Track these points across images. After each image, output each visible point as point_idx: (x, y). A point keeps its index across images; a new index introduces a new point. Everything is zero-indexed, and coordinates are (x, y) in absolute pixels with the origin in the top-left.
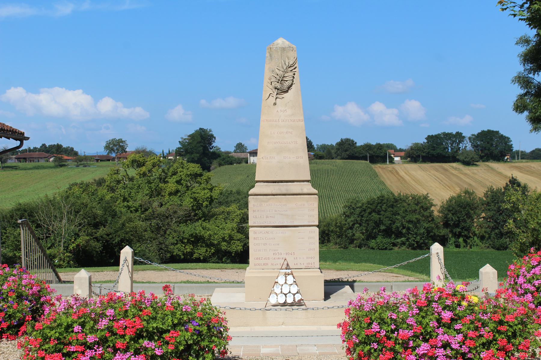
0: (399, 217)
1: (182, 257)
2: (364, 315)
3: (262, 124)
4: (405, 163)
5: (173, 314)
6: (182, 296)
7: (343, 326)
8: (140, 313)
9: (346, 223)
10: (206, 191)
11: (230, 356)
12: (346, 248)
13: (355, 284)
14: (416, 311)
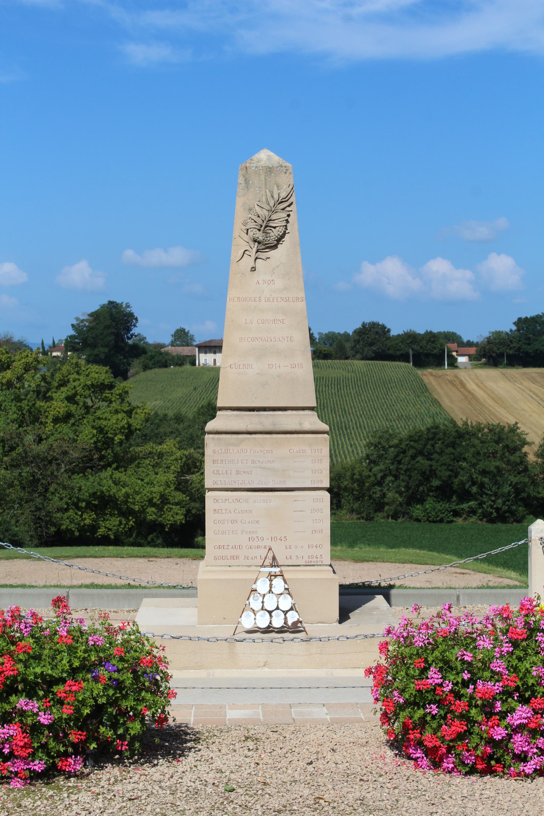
1: (77, 534)
3: (230, 305)
4: (476, 366)
5: (72, 650)
6: (85, 614)
8: (12, 648)
9: (371, 474)
10: (120, 416)
12: (369, 519)
13: (393, 592)
14: (507, 648)
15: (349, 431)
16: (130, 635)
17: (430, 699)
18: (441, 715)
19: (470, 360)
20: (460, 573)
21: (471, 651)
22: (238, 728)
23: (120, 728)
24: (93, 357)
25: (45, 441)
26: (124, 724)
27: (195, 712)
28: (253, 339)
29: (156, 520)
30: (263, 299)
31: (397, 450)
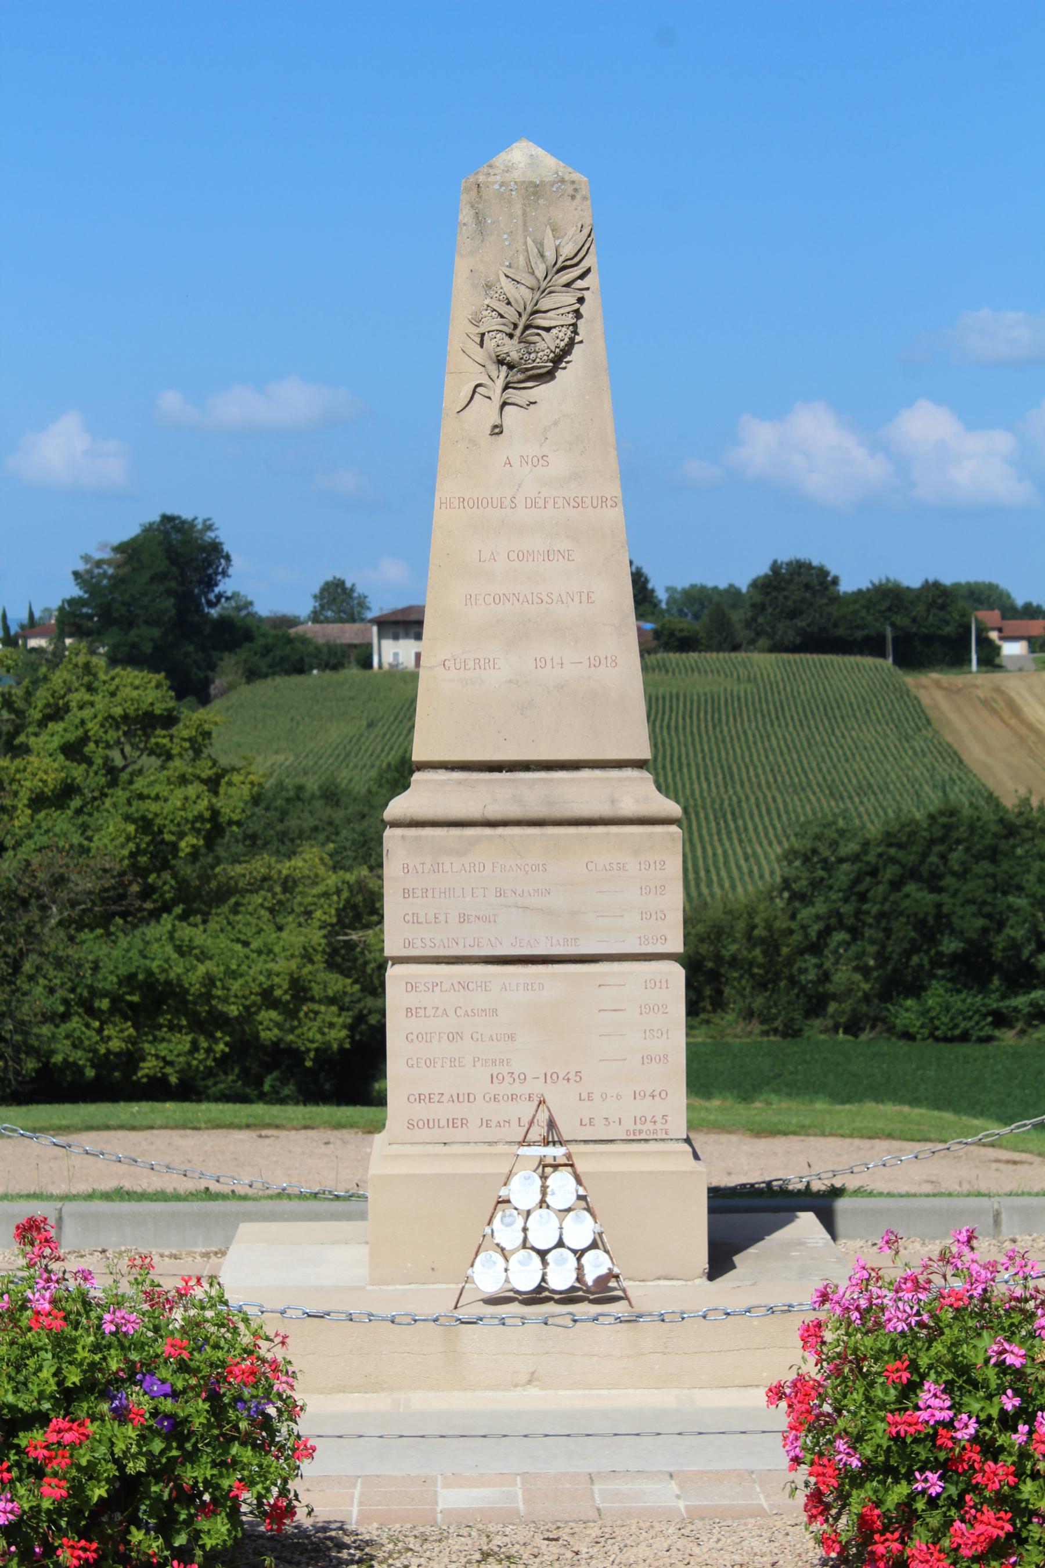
0: (1020, 902)
1: (90, 1073)
2: (881, 1351)
3: (441, 516)
5: (62, 1346)
6: (96, 1261)
7: (794, 1394)
9: (794, 925)
10: (192, 790)
11: (307, 1523)
12: (791, 1032)
13: (841, 1204)
15: (740, 823)
16: (203, 1308)
17: (923, 1457)
18: (950, 1497)
19: (1032, 649)
20: (1008, 1162)
21: (1022, 1342)
22: (464, 1531)
23: (178, 1532)
24: (126, 649)
25: (11, 853)
26: (189, 1521)
27: (362, 1494)
28: (498, 599)
29: (280, 1040)
30: (520, 501)
31: (856, 867)
